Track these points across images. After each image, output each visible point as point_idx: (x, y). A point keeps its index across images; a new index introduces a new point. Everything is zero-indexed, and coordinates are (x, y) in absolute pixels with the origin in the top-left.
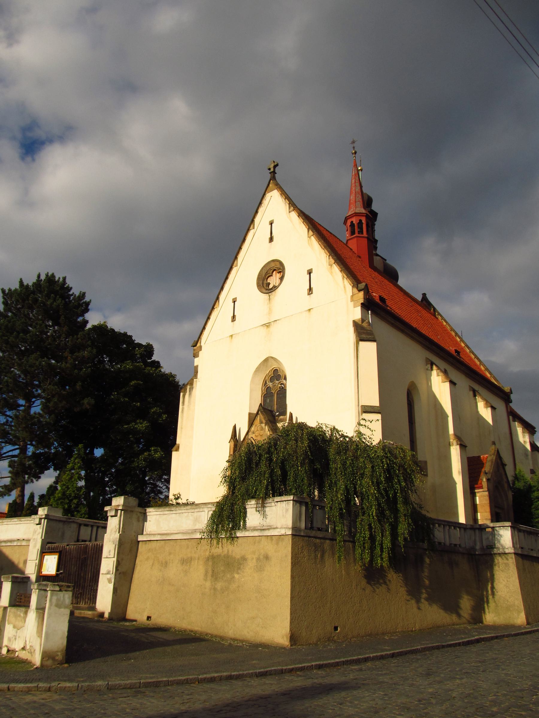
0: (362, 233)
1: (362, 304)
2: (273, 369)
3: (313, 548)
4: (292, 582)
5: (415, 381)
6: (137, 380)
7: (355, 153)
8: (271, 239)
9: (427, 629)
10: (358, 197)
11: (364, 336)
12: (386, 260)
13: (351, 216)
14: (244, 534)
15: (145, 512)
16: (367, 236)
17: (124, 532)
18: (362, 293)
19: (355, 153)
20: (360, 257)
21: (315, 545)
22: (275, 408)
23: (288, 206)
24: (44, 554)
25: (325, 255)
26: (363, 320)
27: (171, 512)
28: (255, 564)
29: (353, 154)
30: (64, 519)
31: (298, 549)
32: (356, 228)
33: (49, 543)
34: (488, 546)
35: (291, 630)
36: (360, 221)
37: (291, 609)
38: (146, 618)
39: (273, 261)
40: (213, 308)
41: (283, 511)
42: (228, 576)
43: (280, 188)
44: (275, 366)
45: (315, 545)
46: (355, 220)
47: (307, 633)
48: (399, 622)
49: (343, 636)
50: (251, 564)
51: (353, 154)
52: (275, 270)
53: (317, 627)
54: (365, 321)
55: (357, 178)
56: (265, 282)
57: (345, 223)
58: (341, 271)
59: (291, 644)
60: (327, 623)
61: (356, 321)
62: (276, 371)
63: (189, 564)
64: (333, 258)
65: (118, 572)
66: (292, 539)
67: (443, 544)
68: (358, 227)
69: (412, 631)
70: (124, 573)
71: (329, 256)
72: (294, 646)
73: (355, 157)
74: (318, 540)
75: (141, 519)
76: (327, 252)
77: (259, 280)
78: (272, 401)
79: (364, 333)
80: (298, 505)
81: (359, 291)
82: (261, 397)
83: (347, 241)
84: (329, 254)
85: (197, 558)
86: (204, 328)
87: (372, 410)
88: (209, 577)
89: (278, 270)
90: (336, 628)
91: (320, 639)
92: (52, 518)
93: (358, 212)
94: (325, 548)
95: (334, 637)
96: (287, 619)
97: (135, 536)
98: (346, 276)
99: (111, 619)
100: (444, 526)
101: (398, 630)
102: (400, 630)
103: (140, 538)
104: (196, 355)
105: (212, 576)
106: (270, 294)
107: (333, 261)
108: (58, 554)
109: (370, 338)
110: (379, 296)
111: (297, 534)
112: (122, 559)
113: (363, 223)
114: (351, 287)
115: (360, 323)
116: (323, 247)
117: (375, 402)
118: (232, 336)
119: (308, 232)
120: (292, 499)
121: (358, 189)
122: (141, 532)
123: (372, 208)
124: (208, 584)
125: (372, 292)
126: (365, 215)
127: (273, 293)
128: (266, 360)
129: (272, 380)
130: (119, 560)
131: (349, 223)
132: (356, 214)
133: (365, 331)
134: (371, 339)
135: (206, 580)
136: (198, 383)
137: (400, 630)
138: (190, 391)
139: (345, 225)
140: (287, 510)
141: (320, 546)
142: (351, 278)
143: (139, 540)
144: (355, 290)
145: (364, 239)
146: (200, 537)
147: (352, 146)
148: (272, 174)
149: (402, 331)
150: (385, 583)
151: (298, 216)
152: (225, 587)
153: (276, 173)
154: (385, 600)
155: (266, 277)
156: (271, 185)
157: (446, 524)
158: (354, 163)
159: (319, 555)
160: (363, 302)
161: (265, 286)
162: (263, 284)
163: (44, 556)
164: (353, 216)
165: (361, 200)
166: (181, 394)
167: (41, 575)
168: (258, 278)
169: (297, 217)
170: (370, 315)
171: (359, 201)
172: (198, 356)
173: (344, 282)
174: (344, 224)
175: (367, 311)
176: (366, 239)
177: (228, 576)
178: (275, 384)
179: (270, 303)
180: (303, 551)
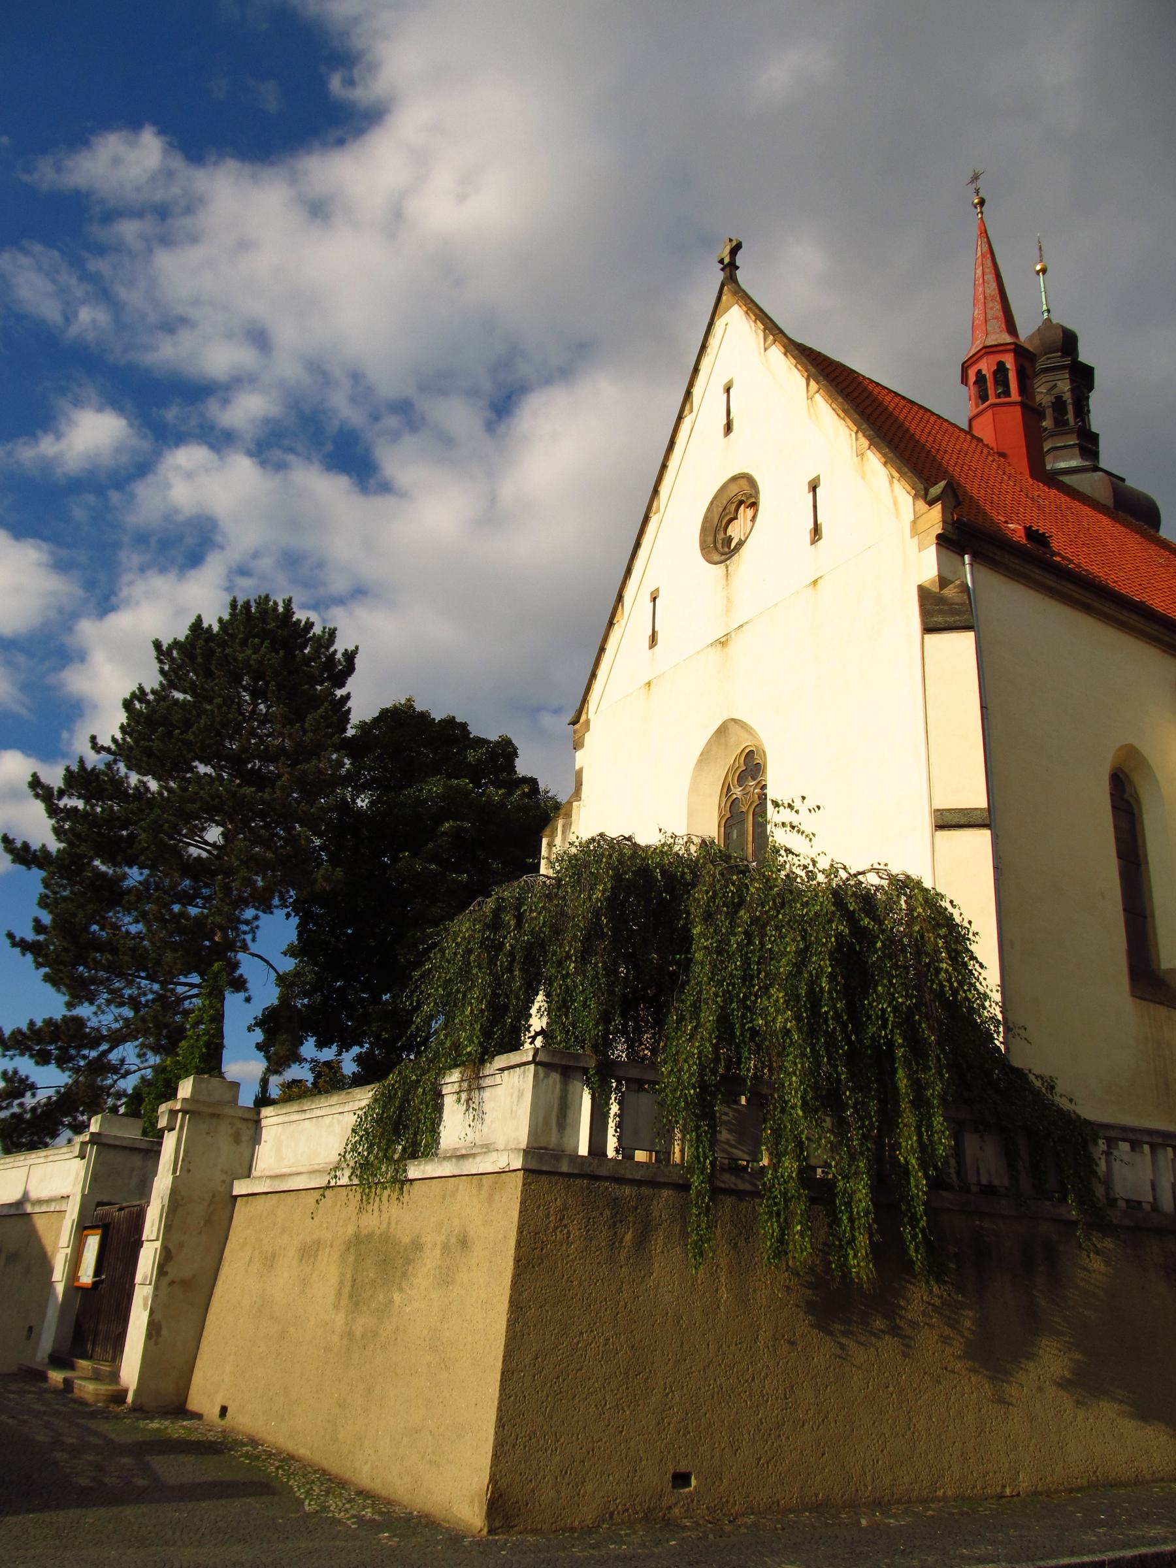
0: (1007, 393)
1: (939, 537)
2: (743, 750)
3: (607, 1212)
4: (512, 1324)
5: (1139, 746)
6: (455, 820)
7: (982, 203)
8: (728, 428)
9: (1064, 1491)
10: (992, 309)
11: (939, 619)
12: (1123, 480)
13: (975, 358)
14: (424, 1172)
15: (256, 1118)
16: (1019, 399)
17: (189, 1171)
18: (938, 508)
19: (982, 203)
20: (1003, 455)
21: (614, 1203)
22: (750, 851)
23: (761, 334)
24: (86, 1232)
25: (847, 431)
26: (943, 581)
27: (303, 1116)
28: (439, 1263)
29: (976, 207)
30: (144, 1146)
31: (548, 1216)
32: (990, 384)
33: (100, 1204)
34: (485, 1153)
35: (493, 1479)
36: (1001, 366)
37: (499, 1409)
38: (217, 1410)
39: (734, 479)
40: (611, 624)
41: (512, 1096)
42: (381, 1297)
43: (743, 298)
44: (746, 742)
45: (614, 1203)
46: (986, 366)
47: (559, 1492)
48: (946, 1465)
49: (708, 1508)
50: (430, 1260)
51: (976, 207)
52: (741, 502)
53: (602, 1475)
54: (952, 582)
55: (989, 262)
56: (721, 536)
57: (964, 380)
58: (885, 464)
59: (490, 1525)
60: (644, 1463)
61: (927, 585)
62: (750, 755)
63: (312, 1259)
64: (865, 436)
65: (167, 1280)
66: (524, 1185)
67: (1147, 1207)
68: (997, 382)
69: (1001, 1496)
70: (186, 1284)
71: (856, 433)
72: (503, 1533)
73: (981, 212)
74: (627, 1190)
75: (245, 1138)
76: (850, 424)
77: (705, 535)
78: (742, 834)
79: (940, 611)
80: (555, 1077)
81: (931, 503)
82: (719, 826)
83: (971, 421)
84: (855, 429)
85: (329, 1243)
86: (593, 675)
87: (963, 821)
88: (345, 1301)
89: (748, 498)
90: (681, 1479)
91: (612, 1514)
92: (111, 1142)
93: (994, 343)
94: (656, 1214)
95: (669, 1508)
96: (487, 1440)
97: (223, 1182)
98: (896, 475)
99: (138, 1409)
100: (1153, 1147)
101: (940, 1493)
102: (949, 1493)
103: (240, 1188)
104: (578, 745)
105: (351, 1297)
106: (728, 562)
107: (865, 443)
108: (100, 1231)
109: (955, 621)
110: (1025, 527)
111: (544, 1168)
112: (181, 1245)
113: (1008, 369)
114: (910, 499)
115: (936, 589)
116: (842, 415)
117: (977, 799)
118: (649, 684)
119: (808, 385)
120: (530, 1059)
121: (992, 288)
122: (246, 1172)
123: (1081, 359)
124: (339, 1319)
125: (1006, 522)
126: (1012, 347)
127: (735, 558)
128: (722, 731)
129: (741, 780)
130: (170, 1246)
131: (972, 378)
132: (988, 350)
133: (946, 608)
134: (958, 624)
135: (336, 1307)
136: (582, 809)
137: (949, 1493)
138: (563, 832)
139: (966, 385)
140: (521, 1094)
141: (636, 1208)
142: (910, 474)
143: (235, 1193)
144: (921, 505)
145: (1011, 409)
146: (324, 1183)
147: (972, 187)
148: (728, 270)
149: (1087, 609)
150: (895, 1331)
151: (785, 354)
152: (371, 1332)
153: (737, 268)
154: (891, 1389)
155: (724, 524)
156: (724, 298)
157: (1160, 1141)
158: (980, 228)
159: (628, 1237)
160: (940, 531)
161: (719, 546)
162: (715, 542)
163: (87, 1236)
164: (981, 357)
165: (1000, 314)
166: (545, 841)
167: (76, 1284)
168: (704, 530)
169: (783, 356)
170: (968, 567)
171: (996, 318)
172: (582, 746)
173: (892, 491)
174: (962, 383)
175: (958, 558)
176: (1018, 409)
177: (381, 1297)
178: (748, 789)
179: (728, 585)
180: (565, 1222)
